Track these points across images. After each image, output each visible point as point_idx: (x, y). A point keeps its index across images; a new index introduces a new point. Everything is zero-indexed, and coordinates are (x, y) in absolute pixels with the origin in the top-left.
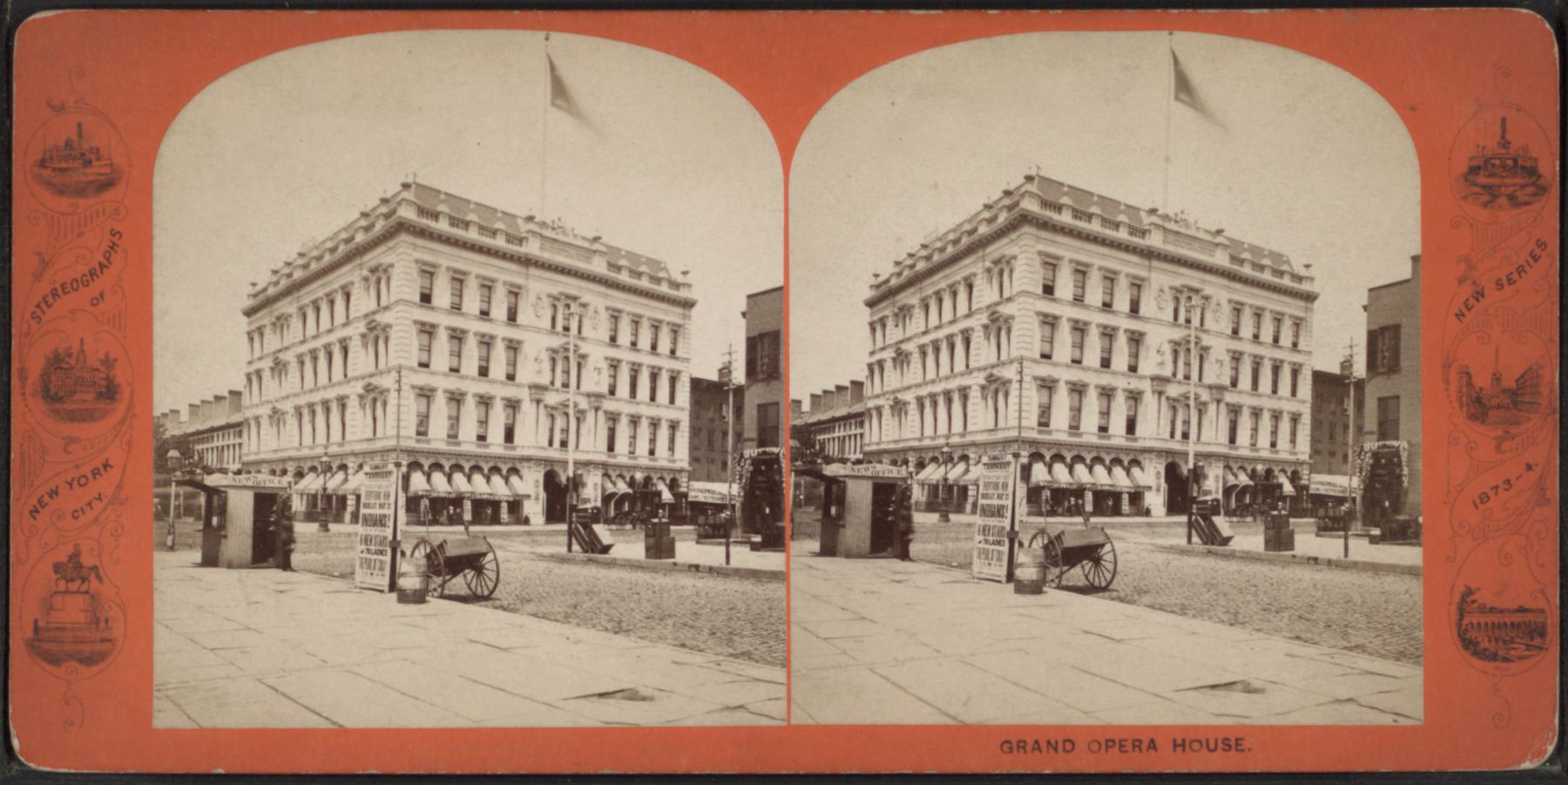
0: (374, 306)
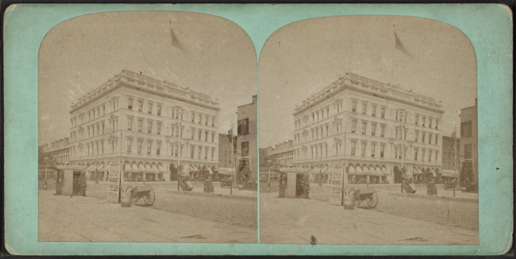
0: (113, 110)
